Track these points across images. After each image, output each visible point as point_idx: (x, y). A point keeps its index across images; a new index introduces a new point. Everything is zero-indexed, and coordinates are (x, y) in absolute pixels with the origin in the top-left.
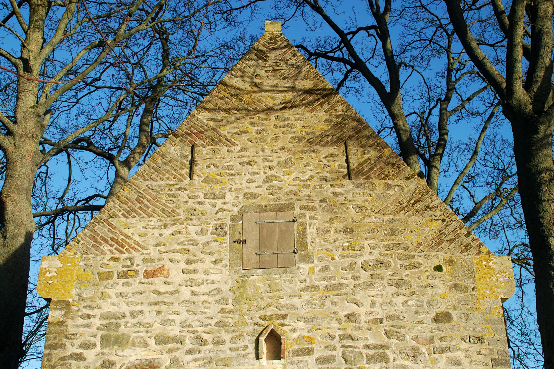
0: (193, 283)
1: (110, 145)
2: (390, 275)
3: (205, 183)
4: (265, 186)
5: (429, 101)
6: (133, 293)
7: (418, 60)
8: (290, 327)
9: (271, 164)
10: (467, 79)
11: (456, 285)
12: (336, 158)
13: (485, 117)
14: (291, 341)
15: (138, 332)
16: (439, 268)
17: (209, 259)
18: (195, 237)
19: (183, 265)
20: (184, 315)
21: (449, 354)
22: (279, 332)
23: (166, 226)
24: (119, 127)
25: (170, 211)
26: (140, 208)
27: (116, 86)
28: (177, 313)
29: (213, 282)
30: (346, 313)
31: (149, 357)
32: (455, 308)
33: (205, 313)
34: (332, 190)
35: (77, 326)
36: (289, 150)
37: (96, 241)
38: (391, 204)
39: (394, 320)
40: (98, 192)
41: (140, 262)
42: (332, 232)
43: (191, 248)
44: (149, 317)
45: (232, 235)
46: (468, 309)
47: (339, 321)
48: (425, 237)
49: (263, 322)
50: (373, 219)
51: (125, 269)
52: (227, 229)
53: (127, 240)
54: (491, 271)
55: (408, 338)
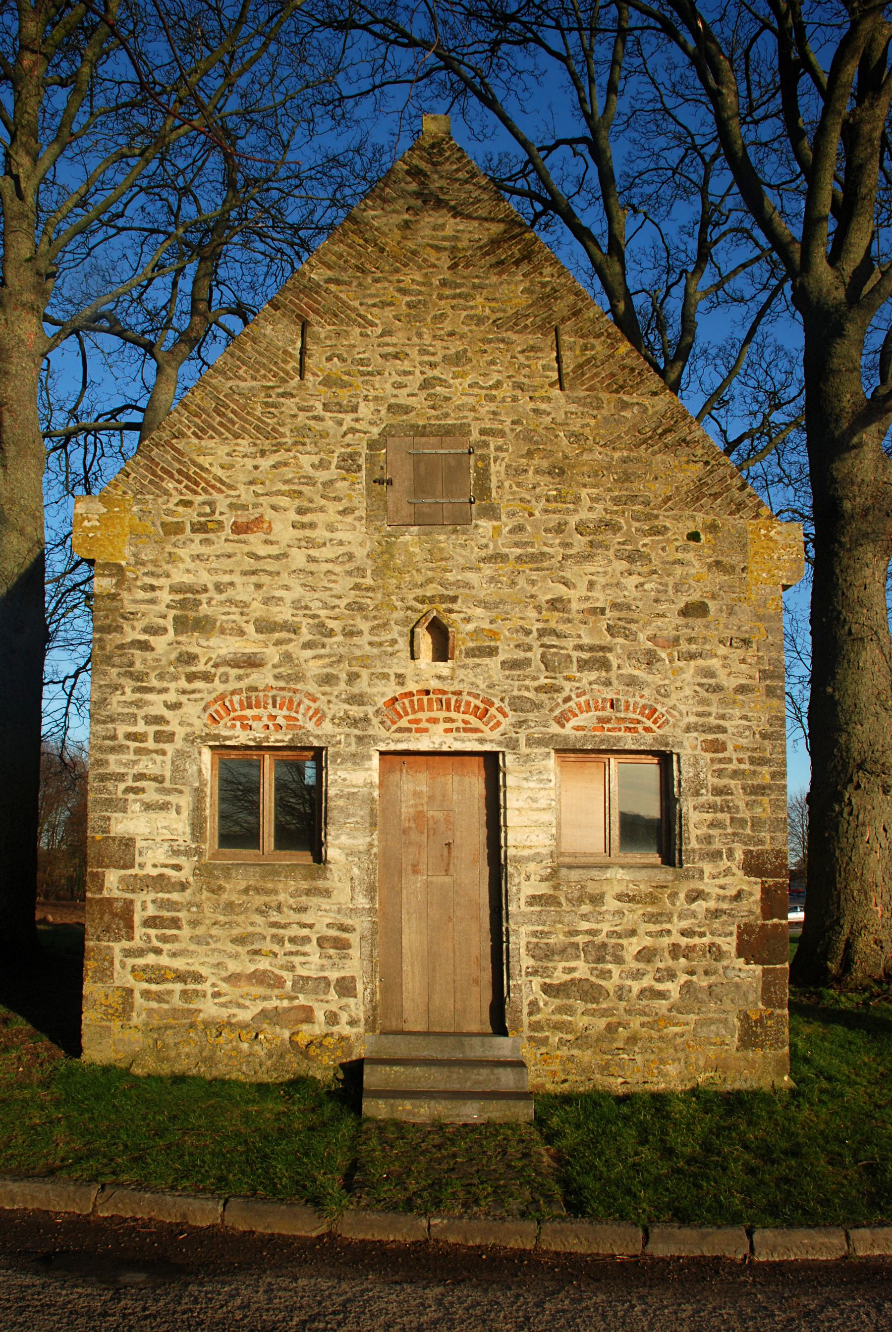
0: (311, 543)
1: (145, 325)
2: (619, 543)
3: (325, 385)
4: (423, 394)
5: (668, 273)
6: (218, 556)
7: (652, 202)
8: (462, 615)
9: (432, 359)
10: (728, 240)
11: (718, 563)
12: (540, 354)
13: (754, 308)
14: (464, 635)
15: (229, 613)
16: (694, 537)
17: (333, 508)
18: (311, 472)
19: (293, 516)
20: (298, 592)
21: (700, 662)
22: (445, 621)
23: (263, 453)
24: (158, 295)
25: (269, 429)
26: (221, 424)
27: (149, 226)
28: (287, 588)
29: (341, 543)
30: (549, 597)
31: (247, 651)
32: (714, 597)
33: (330, 589)
34: (531, 405)
35: (136, 602)
36: (462, 337)
37: (154, 474)
38: (626, 433)
39: (621, 610)
40: (129, 402)
41: (225, 509)
42: (531, 472)
43: (305, 489)
44: (244, 591)
45: (370, 472)
46: (733, 599)
47: (539, 609)
48: (677, 488)
49: (420, 606)
50: (598, 455)
51: (203, 519)
52: (362, 461)
53: (203, 474)
54: (771, 544)
55: (642, 637)
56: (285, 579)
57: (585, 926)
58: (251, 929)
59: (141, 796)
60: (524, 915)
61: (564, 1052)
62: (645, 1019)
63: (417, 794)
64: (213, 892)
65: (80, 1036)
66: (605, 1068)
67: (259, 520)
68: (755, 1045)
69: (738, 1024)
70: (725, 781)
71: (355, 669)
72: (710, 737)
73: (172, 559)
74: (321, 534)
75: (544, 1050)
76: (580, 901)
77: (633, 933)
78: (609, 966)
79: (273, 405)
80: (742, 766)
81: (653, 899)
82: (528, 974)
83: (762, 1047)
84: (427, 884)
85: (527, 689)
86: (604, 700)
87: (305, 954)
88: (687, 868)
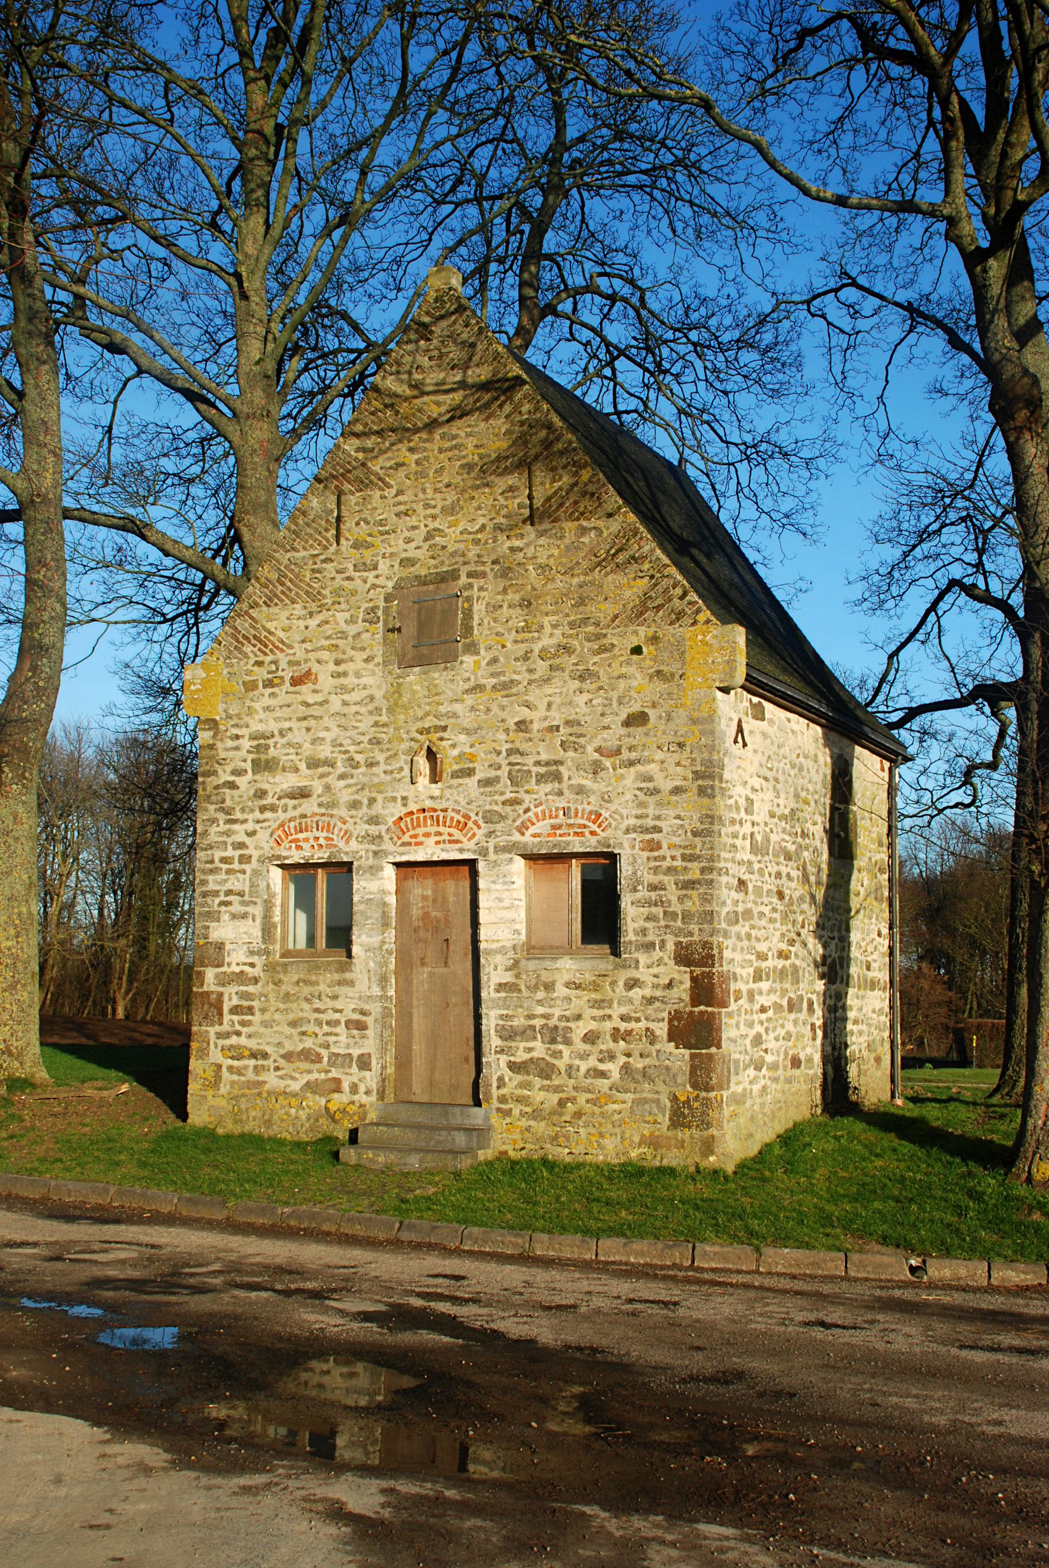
0: (344, 689)
4: (426, 546)
19: (332, 667)
21: (639, 767)
26: (283, 592)
28: (327, 729)
30: (517, 719)
32: (654, 706)
35: (226, 749)
37: (237, 641)
47: (507, 731)
52: (380, 613)
54: (707, 649)
55: (590, 749)
56: (327, 722)
57: (540, 1010)
58: (301, 1014)
59: (230, 908)
60: (493, 1000)
61: (524, 1123)
62: (590, 1096)
63: (424, 898)
64: (275, 984)
65: (186, 1104)
66: (554, 1139)
67: (308, 673)
68: (683, 1125)
69: (668, 1104)
70: (661, 877)
71: (373, 795)
72: (648, 837)
73: (250, 711)
74: (350, 681)
75: (508, 1120)
76: (536, 987)
77: (579, 1017)
78: (561, 1047)
79: (319, 571)
80: (675, 863)
81: (596, 987)
82: (496, 1052)
83: (689, 1127)
84: (431, 975)
85: (496, 803)
86: (557, 809)
87: (336, 1035)
88: (625, 960)
